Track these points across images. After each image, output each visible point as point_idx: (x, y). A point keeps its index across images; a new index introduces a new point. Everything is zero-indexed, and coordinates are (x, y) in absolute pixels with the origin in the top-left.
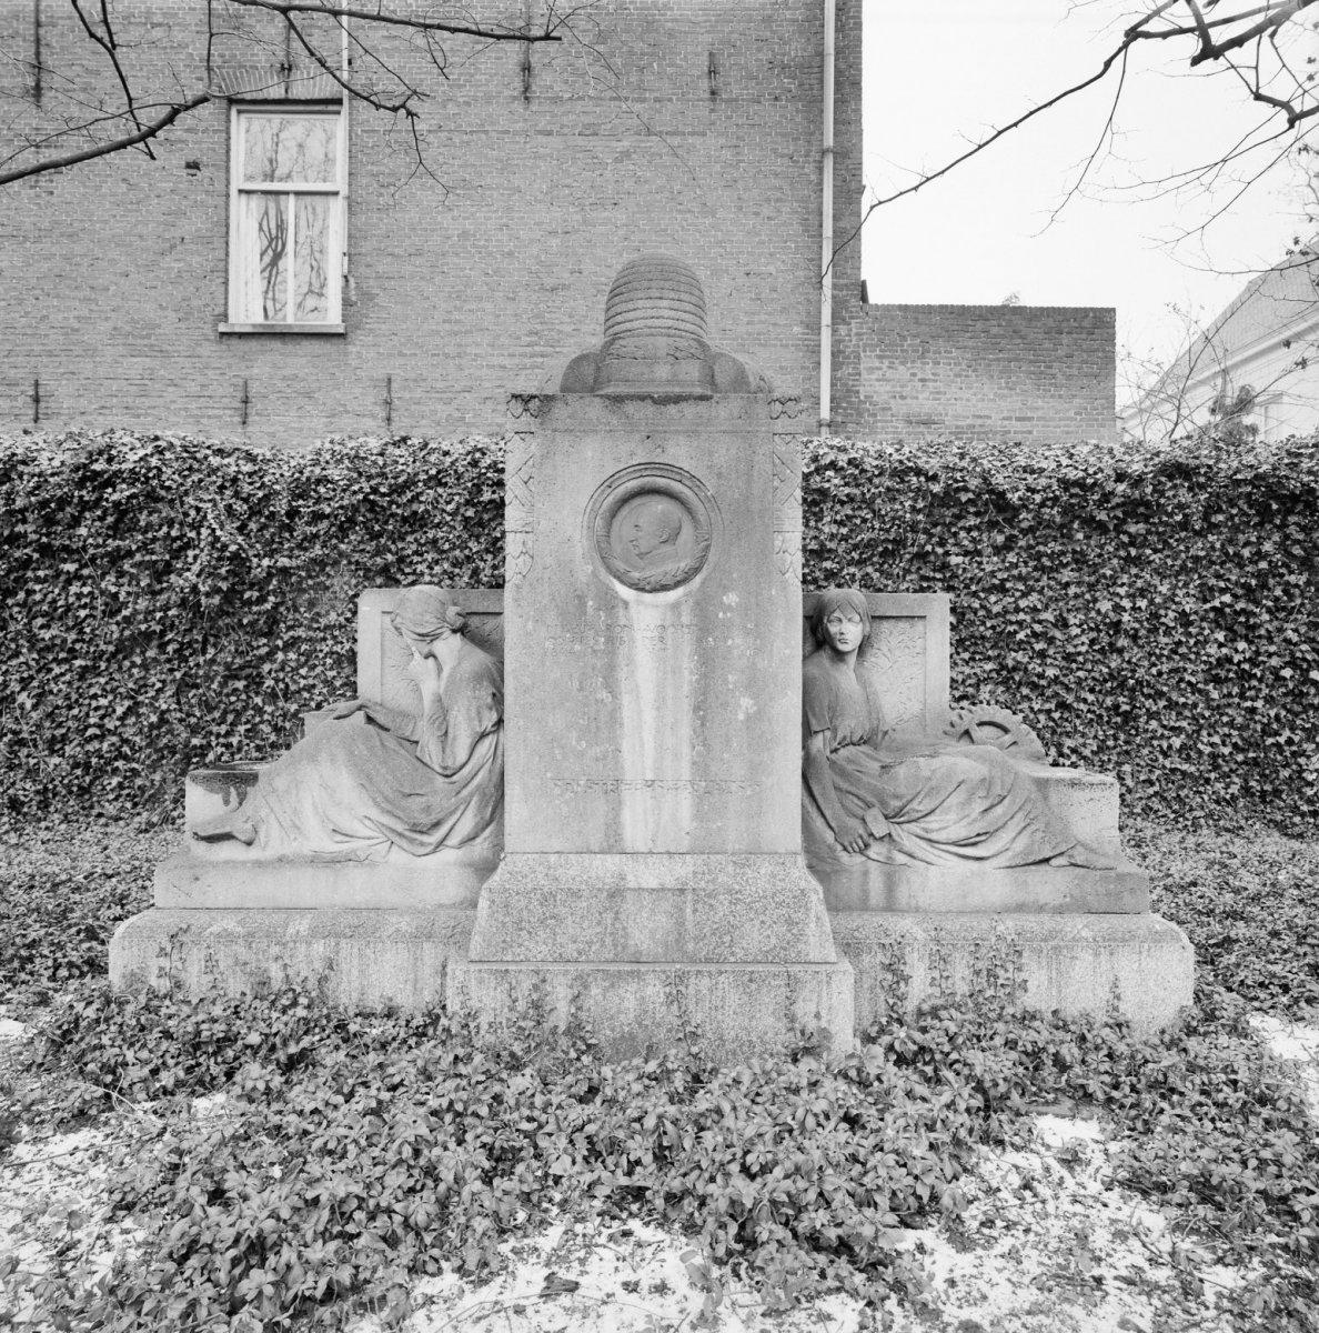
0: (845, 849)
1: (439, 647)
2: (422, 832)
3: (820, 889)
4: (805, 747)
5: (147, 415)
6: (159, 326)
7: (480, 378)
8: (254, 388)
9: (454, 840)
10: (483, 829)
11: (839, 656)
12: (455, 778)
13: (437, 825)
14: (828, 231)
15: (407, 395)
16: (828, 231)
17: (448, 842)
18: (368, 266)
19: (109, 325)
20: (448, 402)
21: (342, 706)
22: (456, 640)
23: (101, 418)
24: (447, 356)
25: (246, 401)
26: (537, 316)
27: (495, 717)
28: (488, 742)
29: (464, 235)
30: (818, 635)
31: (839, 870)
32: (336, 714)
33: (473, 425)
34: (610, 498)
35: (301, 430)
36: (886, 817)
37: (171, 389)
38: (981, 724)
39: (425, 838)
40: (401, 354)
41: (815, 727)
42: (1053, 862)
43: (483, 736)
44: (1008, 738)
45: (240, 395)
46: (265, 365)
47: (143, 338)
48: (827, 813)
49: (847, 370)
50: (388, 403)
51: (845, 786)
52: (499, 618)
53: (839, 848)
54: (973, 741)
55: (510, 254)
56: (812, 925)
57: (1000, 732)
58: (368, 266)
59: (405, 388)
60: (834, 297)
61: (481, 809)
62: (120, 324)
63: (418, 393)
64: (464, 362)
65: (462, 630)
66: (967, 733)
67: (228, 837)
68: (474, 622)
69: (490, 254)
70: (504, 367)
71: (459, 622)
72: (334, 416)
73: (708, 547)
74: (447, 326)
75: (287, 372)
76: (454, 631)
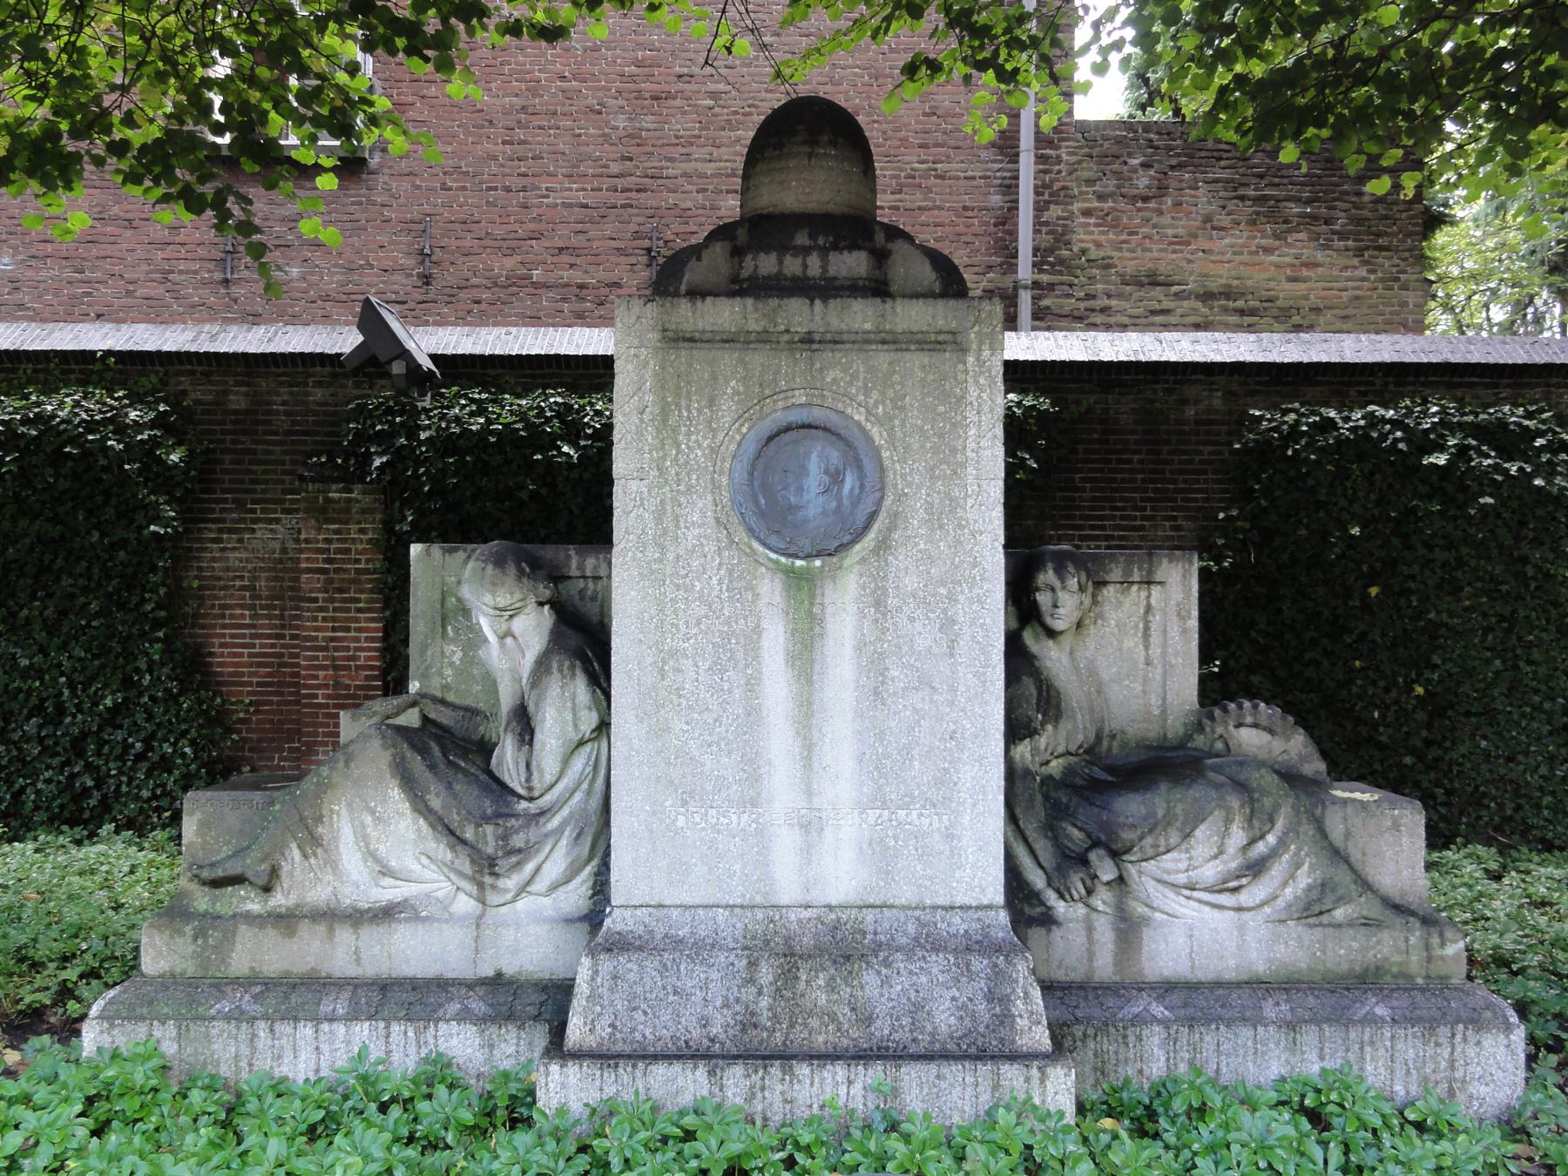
0: (1062, 897)
1: (518, 625)
5: (93, 269)
9: (540, 885)
11: (1052, 634)
15: (453, 243)
24: (508, 190)
40: (444, 188)
43: (581, 743)
70: (585, 206)
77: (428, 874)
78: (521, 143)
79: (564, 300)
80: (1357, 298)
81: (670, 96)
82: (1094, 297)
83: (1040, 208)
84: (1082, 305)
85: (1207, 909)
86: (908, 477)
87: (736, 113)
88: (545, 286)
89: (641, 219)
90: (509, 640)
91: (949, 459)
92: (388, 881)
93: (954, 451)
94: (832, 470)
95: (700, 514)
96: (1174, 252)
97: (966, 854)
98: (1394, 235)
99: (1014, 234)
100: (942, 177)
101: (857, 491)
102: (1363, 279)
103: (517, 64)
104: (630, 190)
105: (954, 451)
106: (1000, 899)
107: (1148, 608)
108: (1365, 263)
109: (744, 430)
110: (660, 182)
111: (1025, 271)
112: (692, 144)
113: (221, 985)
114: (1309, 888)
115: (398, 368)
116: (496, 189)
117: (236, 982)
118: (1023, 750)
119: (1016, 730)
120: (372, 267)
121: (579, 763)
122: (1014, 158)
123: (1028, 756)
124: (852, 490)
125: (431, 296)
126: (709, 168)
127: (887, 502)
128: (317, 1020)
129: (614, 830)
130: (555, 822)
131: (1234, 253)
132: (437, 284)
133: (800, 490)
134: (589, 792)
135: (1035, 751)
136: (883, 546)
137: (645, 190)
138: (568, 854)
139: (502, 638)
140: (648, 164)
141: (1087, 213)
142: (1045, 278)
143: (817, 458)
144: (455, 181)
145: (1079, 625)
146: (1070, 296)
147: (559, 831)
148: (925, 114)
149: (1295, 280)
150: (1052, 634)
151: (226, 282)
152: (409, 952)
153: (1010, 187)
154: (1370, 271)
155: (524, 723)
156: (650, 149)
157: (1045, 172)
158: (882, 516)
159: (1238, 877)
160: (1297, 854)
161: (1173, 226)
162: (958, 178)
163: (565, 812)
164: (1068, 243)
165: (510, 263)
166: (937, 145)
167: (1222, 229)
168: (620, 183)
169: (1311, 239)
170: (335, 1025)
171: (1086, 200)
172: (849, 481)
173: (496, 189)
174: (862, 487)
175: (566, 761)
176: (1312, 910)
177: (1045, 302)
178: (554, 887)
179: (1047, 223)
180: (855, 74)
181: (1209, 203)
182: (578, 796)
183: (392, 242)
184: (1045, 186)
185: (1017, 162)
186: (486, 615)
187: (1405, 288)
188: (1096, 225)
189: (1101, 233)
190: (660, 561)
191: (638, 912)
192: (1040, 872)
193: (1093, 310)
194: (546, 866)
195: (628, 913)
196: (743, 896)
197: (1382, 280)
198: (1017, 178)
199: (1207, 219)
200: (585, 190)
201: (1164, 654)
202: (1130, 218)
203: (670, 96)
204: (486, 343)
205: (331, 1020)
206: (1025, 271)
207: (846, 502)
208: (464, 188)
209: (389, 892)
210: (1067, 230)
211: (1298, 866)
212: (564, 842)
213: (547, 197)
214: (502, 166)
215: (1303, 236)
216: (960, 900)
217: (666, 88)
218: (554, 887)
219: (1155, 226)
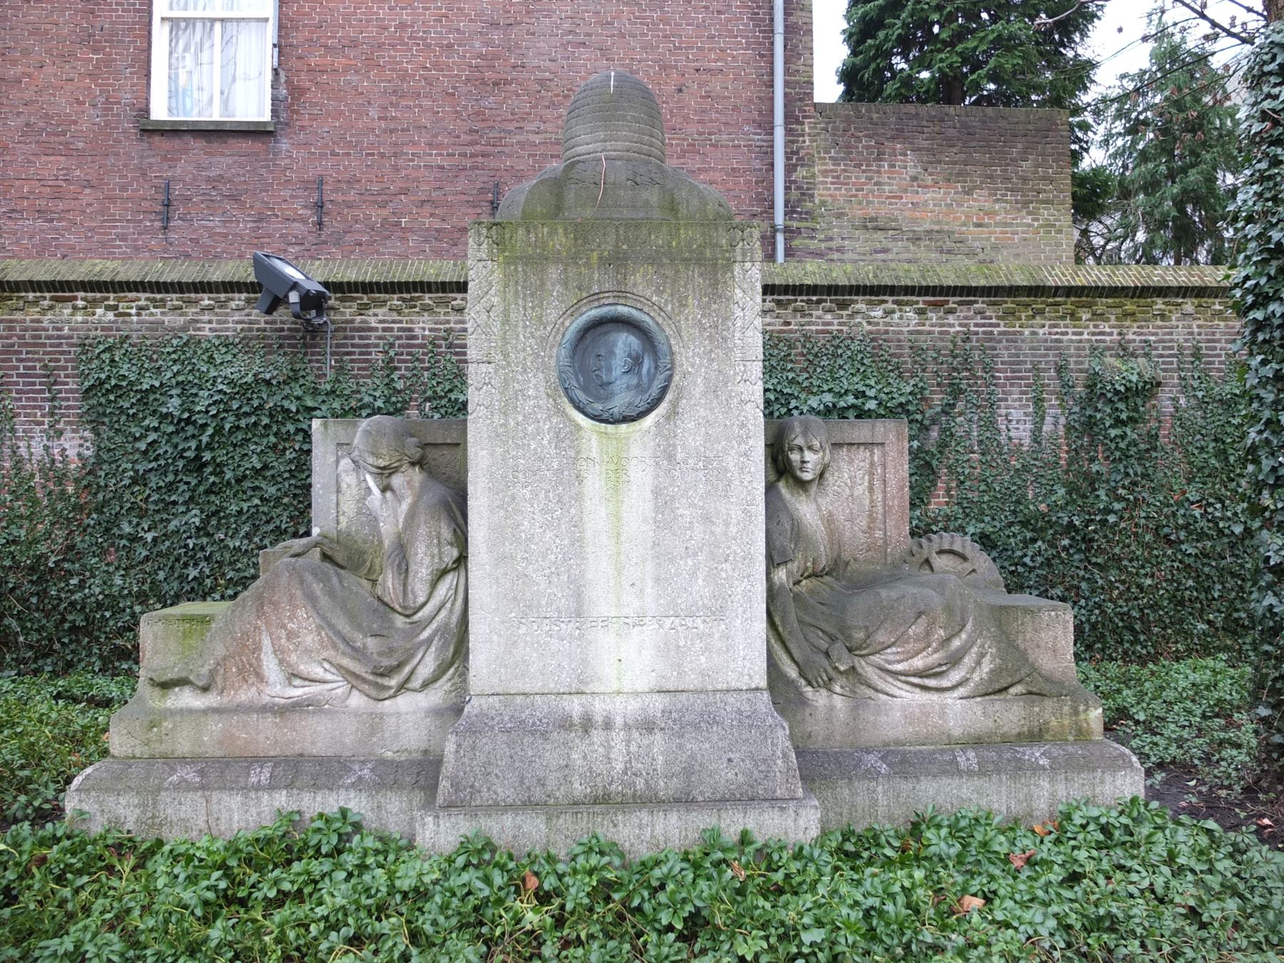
0: (810, 684)
1: (397, 481)
2: (382, 675)
3: (786, 725)
4: (769, 579)
5: (59, 220)
6: (75, 123)
7: (416, 180)
8: (177, 190)
9: (416, 683)
10: (444, 672)
11: (802, 485)
12: (416, 618)
13: (400, 666)
14: (779, 133)
15: (340, 198)
16: (779, 133)
17: (409, 686)
18: (299, 58)
19: (21, 121)
20: (383, 206)
21: (298, 544)
22: (417, 475)
23: (9, 223)
24: (382, 155)
25: (168, 204)
26: (477, 113)
27: (455, 553)
28: (449, 579)
29: (402, 26)
30: (780, 465)
31: (802, 701)
32: (292, 552)
33: (411, 230)
34: (575, 325)
35: (225, 236)
36: (850, 650)
37: (87, 191)
38: (941, 552)
39: (385, 681)
40: (334, 154)
41: (777, 560)
42: (1012, 690)
43: (444, 573)
44: (968, 566)
45: (161, 197)
46: (190, 163)
47: (57, 135)
48: (792, 646)
49: (801, 173)
50: (319, 206)
51: (808, 619)
52: (459, 451)
53: (803, 682)
54: (932, 569)
55: (450, 46)
56: (779, 762)
57: (959, 560)
58: (299, 58)
59: (336, 191)
60: (786, 95)
61: (444, 647)
62: (32, 120)
63: (352, 196)
64: (401, 162)
65: (419, 463)
66: (927, 561)
67: (182, 682)
68: (433, 454)
69: (428, 46)
70: (442, 167)
71: (417, 453)
72: (261, 220)
73: (671, 376)
74: (383, 124)
75: (213, 173)
76: (413, 464)
77: (329, 677)
78: (394, 118)
79: (426, 241)
80: (1025, 240)
81: (507, 83)
82: (831, 239)
83: (790, 169)
84: (823, 245)
85: (917, 690)
86: (690, 358)
87: (557, 95)
88: (411, 230)
89: (485, 179)
90: (388, 494)
91: (718, 335)
92: (297, 682)
93: (725, 339)
94: (634, 354)
95: (537, 387)
96: (891, 204)
97: (740, 651)
98: (1050, 191)
99: (771, 187)
100: (715, 146)
101: (653, 370)
102: (1029, 225)
103: (389, 56)
104: (477, 156)
105: (725, 339)
106: (763, 683)
107: (872, 464)
108: (1029, 213)
109: (567, 324)
110: (499, 149)
111: (780, 219)
112: (524, 119)
113: (172, 761)
114: (992, 671)
115: (294, 297)
116: (373, 154)
117: (183, 759)
118: (781, 575)
119: (773, 559)
120: (277, 216)
121: (443, 589)
122: (771, 132)
123: (784, 577)
124: (649, 370)
125: (323, 238)
126: (537, 139)
127: (676, 378)
128: (246, 789)
129: (471, 638)
130: (426, 634)
131: (935, 205)
132: (326, 231)
133: (609, 370)
134: (451, 610)
135: (789, 574)
136: (673, 414)
137: (488, 156)
138: (436, 659)
139: (384, 490)
140: (491, 135)
141: (825, 173)
142: (795, 224)
143: (624, 342)
144: (342, 148)
145: (821, 475)
146: (813, 238)
147: (429, 641)
148: (702, 97)
149: (978, 225)
150: (802, 485)
151: (165, 228)
152: (317, 736)
153: (769, 152)
154: (1034, 220)
155: (402, 551)
156: (491, 124)
157: (793, 142)
158: (669, 397)
159: (940, 665)
160: (982, 646)
161: (889, 184)
162: (727, 146)
163: (434, 625)
164: (812, 196)
165: (385, 212)
166: (711, 121)
167: (927, 187)
168: (469, 150)
169: (990, 195)
170: (260, 793)
171: (825, 164)
172: (647, 364)
173: (373, 154)
174: (656, 368)
175: (434, 585)
176: (994, 690)
177: (796, 243)
178: (426, 685)
179: (795, 182)
180: (649, 66)
181: (915, 166)
182: (443, 613)
183: (292, 197)
184: (793, 153)
185: (772, 134)
186: (371, 473)
187: (1060, 232)
188: (832, 183)
189: (836, 189)
190: (504, 425)
191: (491, 699)
192: (794, 666)
193: (831, 249)
194: (420, 668)
195: (483, 701)
196: (570, 686)
197: (1041, 226)
198: (772, 147)
199: (914, 179)
200: (441, 155)
201: (885, 498)
202: (857, 178)
203: (507, 83)
204: (366, 272)
205: (257, 790)
206: (780, 219)
207: (645, 379)
208: (349, 154)
209: (298, 692)
210: (812, 186)
211: (983, 655)
212: (433, 649)
213: (413, 160)
214: (377, 136)
215: (985, 192)
216: (734, 685)
217: (505, 76)
218: (426, 685)
219: (876, 184)
